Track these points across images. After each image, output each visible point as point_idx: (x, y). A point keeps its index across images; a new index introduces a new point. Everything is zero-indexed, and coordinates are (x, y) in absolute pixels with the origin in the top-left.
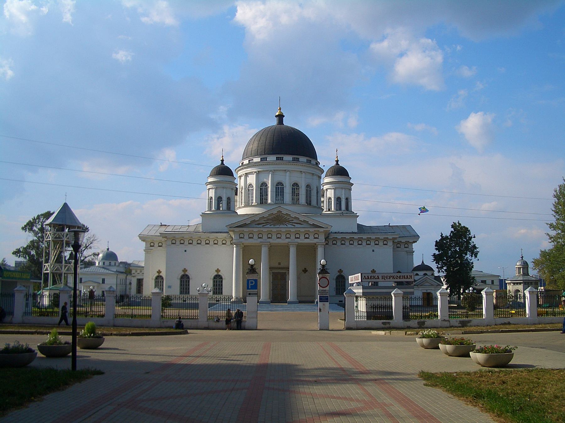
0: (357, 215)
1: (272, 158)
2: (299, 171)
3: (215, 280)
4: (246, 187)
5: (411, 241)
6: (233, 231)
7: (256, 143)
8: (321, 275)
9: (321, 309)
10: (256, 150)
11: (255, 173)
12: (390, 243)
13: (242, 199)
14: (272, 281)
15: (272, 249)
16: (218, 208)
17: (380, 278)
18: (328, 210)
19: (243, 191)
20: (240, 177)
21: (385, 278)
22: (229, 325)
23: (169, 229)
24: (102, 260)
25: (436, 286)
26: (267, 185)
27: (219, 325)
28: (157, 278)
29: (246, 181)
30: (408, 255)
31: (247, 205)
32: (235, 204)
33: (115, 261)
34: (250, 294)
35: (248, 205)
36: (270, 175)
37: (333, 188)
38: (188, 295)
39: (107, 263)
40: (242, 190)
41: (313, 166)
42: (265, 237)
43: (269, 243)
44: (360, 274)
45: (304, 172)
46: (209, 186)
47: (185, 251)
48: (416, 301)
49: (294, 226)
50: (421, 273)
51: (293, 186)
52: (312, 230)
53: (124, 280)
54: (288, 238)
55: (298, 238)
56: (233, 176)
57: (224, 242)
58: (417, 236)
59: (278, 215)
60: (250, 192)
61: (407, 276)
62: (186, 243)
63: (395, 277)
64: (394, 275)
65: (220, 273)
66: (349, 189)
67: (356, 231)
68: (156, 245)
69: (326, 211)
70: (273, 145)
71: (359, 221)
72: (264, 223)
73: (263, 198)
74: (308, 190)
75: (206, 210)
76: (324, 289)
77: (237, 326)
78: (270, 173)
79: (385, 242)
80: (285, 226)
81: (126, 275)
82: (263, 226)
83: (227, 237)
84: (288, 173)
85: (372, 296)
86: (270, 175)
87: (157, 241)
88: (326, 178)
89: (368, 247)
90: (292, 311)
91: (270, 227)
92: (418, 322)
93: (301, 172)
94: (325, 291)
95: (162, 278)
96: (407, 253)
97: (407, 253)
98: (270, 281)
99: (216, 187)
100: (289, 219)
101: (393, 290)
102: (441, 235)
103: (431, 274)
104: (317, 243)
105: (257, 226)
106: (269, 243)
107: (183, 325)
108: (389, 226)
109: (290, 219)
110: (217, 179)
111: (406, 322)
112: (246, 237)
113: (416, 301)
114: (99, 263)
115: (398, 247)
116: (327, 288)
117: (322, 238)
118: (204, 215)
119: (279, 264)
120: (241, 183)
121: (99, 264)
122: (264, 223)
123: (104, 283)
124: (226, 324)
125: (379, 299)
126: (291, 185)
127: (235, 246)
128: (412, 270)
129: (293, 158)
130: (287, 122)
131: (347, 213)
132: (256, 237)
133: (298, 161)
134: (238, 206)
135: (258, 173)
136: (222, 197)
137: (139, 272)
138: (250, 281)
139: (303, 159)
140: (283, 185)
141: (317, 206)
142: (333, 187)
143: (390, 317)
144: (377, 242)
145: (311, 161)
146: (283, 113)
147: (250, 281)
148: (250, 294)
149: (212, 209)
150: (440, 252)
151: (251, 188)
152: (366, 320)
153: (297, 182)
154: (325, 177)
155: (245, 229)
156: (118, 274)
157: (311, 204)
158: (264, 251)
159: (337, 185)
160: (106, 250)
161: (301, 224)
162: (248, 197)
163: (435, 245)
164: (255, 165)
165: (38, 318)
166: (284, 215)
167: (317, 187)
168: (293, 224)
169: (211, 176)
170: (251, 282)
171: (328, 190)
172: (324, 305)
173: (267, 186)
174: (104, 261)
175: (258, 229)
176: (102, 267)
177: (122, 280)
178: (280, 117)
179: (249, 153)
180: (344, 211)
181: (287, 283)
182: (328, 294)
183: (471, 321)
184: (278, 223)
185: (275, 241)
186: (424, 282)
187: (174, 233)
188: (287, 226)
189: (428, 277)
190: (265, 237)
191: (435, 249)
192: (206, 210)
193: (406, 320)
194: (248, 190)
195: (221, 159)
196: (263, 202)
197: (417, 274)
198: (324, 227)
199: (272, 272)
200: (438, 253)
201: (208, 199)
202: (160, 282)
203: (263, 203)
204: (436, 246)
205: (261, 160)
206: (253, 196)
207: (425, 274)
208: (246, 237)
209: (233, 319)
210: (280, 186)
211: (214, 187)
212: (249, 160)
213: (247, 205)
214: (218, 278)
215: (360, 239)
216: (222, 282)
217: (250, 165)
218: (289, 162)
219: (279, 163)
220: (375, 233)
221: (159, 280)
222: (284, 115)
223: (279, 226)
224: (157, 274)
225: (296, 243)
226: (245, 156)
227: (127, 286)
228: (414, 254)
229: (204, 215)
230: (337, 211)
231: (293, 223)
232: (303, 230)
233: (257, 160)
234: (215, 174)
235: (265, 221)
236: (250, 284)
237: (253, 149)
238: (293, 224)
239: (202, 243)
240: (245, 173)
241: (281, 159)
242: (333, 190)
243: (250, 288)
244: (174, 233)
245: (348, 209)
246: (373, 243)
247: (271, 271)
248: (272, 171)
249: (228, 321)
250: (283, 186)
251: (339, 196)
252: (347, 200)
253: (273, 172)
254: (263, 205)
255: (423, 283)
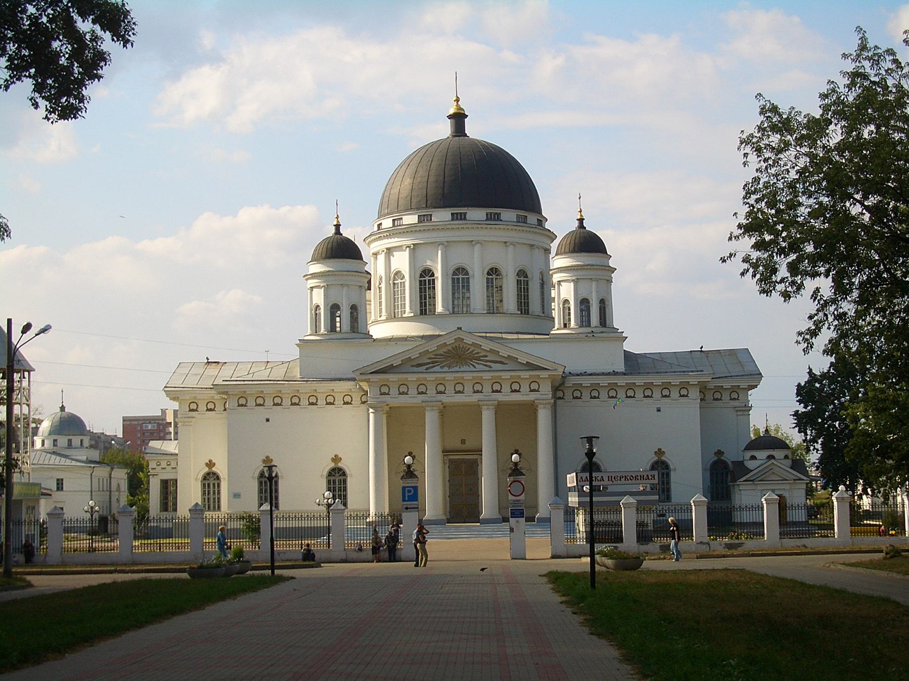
0: (624, 335)
1: (442, 216)
2: (501, 242)
3: (332, 478)
4: (390, 277)
5: (743, 385)
6: (368, 381)
7: (408, 181)
8: (512, 478)
9: (513, 529)
10: (406, 197)
11: (408, 249)
12: (695, 394)
13: (380, 303)
14: (448, 479)
15: (445, 412)
16: (332, 328)
17: (606, 479)
18: (562, 326)
19: (383, 286)
20: (376, 254)
21: (613, 480)
22: (377, 555)
23: (226, 374)
24: (50, 434)
25: (792, 482)
26: (433, 275)
27: (363, 555)
28: (205, 477)
29: (388, 264)
30: (737, 415)
31: (393, 317)
32: (366, 309)
33: (82, 437)
34: (407, 508)
35: (395, 317)
36: (440, 252)
37: (573, 281)
38: (219, 513)
39: (63, 441)
40: (380, 284)
41: (532, 230)
42: (432, 391)
43: (441, 403)
44: (575, 473)
45: (511, 244)
46: (312, 282)
47: (268, 420)
48: (643, 514)
49: (490, 367)
50: (762, 455)
51: (488, 274)
52: (525, 375)
53: (105, 480)
54: (478, 392)
55: (497, 391)
56: (362, 259)
57: (347, 399)
58: (756, 374)
59: (456, 346)
60: (398, 288)
61: (648, 476)
62: (269, 402)
63: (628, 478)
64: (627, 475)
65: (340, 465)
66: (608, 280)
67: (620, 367)
68: (202, 408)
69: (558, 329)
70: (444, 186)
71: (628, 346)
72: (429, 363)
73: (425, 303)
74: (521, 280)
75: (307, 332)
76: (518, 498)
77: (390, 555)
78: (439, 248)
79: (684, 392)
80: (472, 369)
81: (109, 469)
82: (427, 369)
83: (353, 390)
84: (477, 247)
85: (603, 508)
86: (440, 252)
87: (204, 399)
88: (557, 257)
89: (647, 401)
90: (489, 537)
91: (441, 370)
92: (660, 546)
93: (506, 243)
94: (519, 501)
95: (218, 478)
96: (737, 411)
97: (737, 411)
98: (444, 478)
99: (327, 285)
100: (478, 353)
101: (622, 497)
102: (808, 370)
103: (784, 455)
104: (536, 401)
105: (415, 369)
106: (441, 403)
107: (314, 556)
108: (701, 351)
109: (480, 355)
110: (328, 267)
111: (643, 547)
112: (394, 391)
113: (754, 512)
114: (43, 442)
115: (717, 399)
116: (522, 497)
117: (546, 390)
118: (303, 344)
119: (463, 442)
120: (377, 268)
121: (43, 444)
122: (429, 363)
123: (62, 488)
124: (373, 554)
125: (614, 512)
126: (486, 272)
127: (371, 410)
128: (745, 449)
129: (487, 214)
130: (474, 130)
131: (602, 332)
132: (413, 391)
133: (499, 219)
134: (373, 318)
135: (414, 249)
136: (341, 306)
137: (164, 464)
138: (407, 489)
139: (508, 215)
140: (467, 273)
141: (543, 315)
142: (574, 278)
143: (620, 540)
144: (666, 392)
145: (526, 216)
146: (464, 110)
147: (407, 489)
148: (407, 508)
149: (320, 331)
150: (809, 408)
151: (400, 281)
152: (585, 543)
153: (494, 265)
154: (556, 255)
155: (392, 377)
156: (94, 467)
157: (528, 310)
158: (431, 419)
159: (581, 273)
160: (59, 410)
161: (504, 364)
162: (394, 298)
163: (796, 394)
164: (409, 230)
165: (89, 554)
166: (469, 347)
167: (541, 273)
168: (488, 363)
169: (315, 259)
170: (408, 490)
171: (562, 283)
172: (518, 522)
173: (434, 276)
174: (56, 437)
175: (417, 376)
176: (52, 451)
177: (101, 480)
178: (459, 118)
179: (393, 205)
180: (595, 327)
181: (479, 481)
182: (523, 505)
183: (743, 543)
184: (457, 363)
185: (450, 398)
186: (767, 474)
187: (242, 383)
188: (475, 367)
189: (775, 463)
190: (432, 391)
191: (797, 401)
192: (307, 332)
193: (641, 543)
194: (394, 284)
195: (335, 223)
196: (426, 310)
197: (753, 458)
198: (549, 368)
199: (449, 460)
200: (804, 410)
201: (311, 310)
202: (214, 484)
203: (426, 314)
204: (798, 394)
205: (420, 221)
206: (404, 297)
207: (771, 457)
208: (394, 391)
209: (383, 547)
210: (461, 276)
211: (322, 285)
212: (393, 220)
213: (393, 316)
214: (337, 475)
215: (631, 387)
216: (345, 481)
217: (397, 230)
218: (478, 223)
219: (457, 226)
220: (660, 373)
221: (210, 480)
222: (466, 114)
223: (460, 368)
224: (206, 470)
225: (495, 401)
226: (385, 209)
227: (112, 493)
228: (750, 412)
229: (303, 344)
230: (582, 328)
231: (487, 361)
232: (506, 375)
233: (410, 219)
234: (324, 256)
235: (430, 358)
236: (407, 494)
237: (400, 196)
238: (488, 363)
239: (301, 403)
240: (387, 249)
241: (462, 217)
242: (572, 284)
243: (407, 499)
244: (242, 383)
245: (605, 323)
246: (657, 394)
247: (446, 458)
248: (443, 244)
249: (375, 550)
250: (468, 275)
251: (585, 295)
252: (602, 304)
253: (446, 247)
254: (426, 316)
255: (764, 476)
